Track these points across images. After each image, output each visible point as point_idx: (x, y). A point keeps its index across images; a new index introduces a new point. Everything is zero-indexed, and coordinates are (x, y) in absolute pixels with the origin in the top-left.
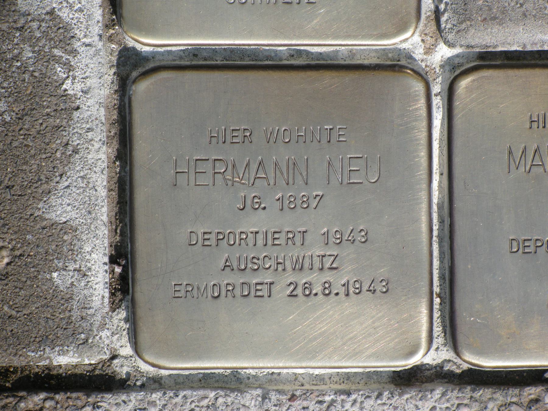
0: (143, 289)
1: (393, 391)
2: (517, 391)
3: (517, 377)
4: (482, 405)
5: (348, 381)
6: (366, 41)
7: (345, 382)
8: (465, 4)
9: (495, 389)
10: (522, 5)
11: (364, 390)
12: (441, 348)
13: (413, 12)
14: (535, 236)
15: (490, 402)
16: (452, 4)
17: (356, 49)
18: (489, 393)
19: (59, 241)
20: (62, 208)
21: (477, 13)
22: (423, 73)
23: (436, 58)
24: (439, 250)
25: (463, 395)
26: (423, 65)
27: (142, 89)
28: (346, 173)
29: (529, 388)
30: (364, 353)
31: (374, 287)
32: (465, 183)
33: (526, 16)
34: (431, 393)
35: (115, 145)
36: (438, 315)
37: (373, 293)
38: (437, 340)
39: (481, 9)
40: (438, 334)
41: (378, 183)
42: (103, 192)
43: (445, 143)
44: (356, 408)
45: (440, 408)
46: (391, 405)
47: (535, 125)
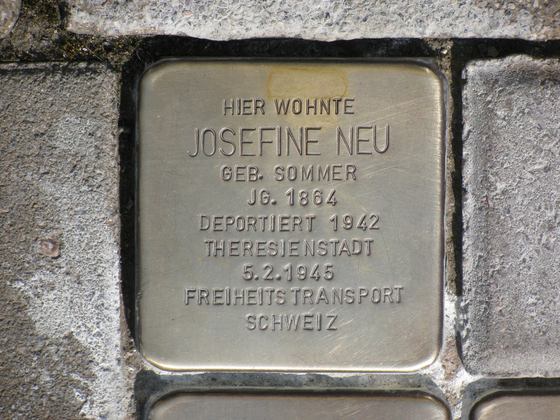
13: (435, 339)
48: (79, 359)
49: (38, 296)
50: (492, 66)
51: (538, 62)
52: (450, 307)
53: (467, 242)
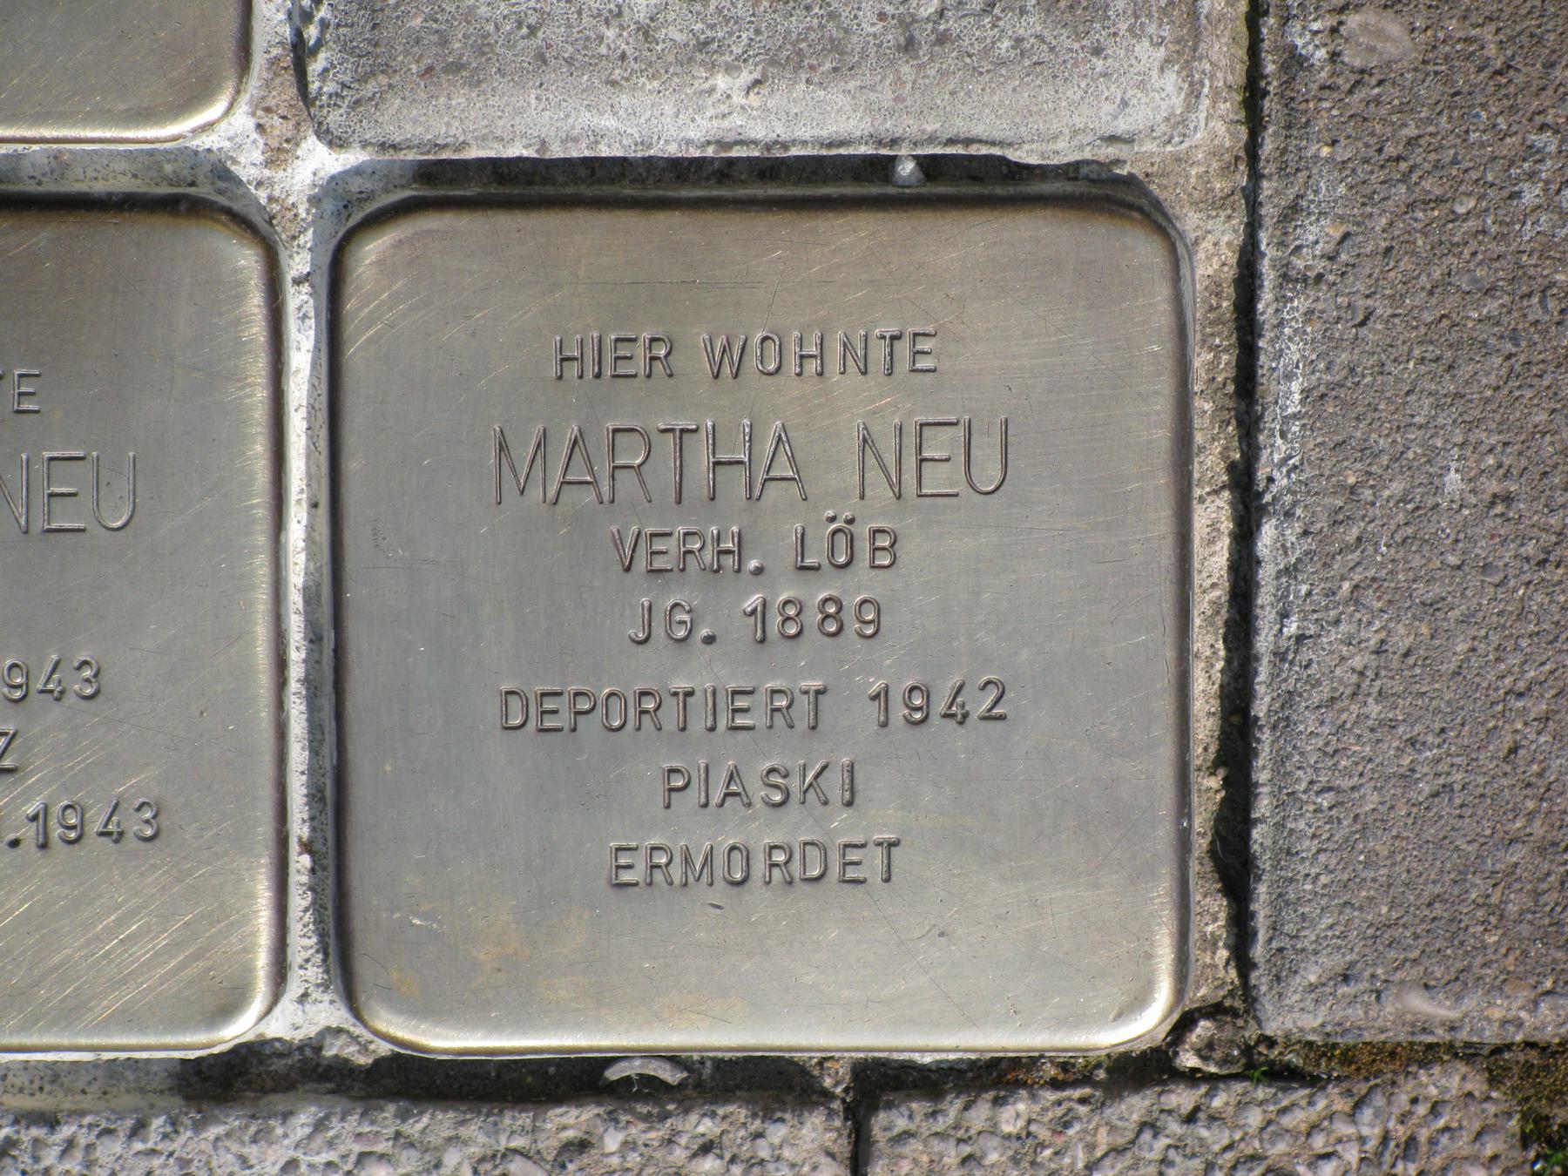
1: (177, 1117)
2: (525, 1118)
3: (529, 1079)
4: (427, 1158)
5: (55, 1087)
6: (94, 128)
7: (47, 1087)
8: (375, 26)
9: (465, 1113)
10: (533, 31)
11: (96, 1113)
12: (314, 996)
13: (229, 49)
14: (572, 683)
15: (451, 1149)
16: (338, 25)
17: (70, 151)
18: (447, 1124)
21: (407, 53)
22: (258, 220)
23: (297, 178)
24: (309, 720)
25: (375, 1128)
26: (262, 195)
28: (39, 501)
29: (558, 1111)
30: (92, 1009)
31: (118, 825)
32: (375, 531)
33: (545, 62)
34: (284, 1123)
36: (305, 903)
37: (117, 841)
38: (302, 972)
39: (418, 41)
40: (306, 955)
41: (129, 531)
43: (323, 416)
44: (73, 1165)
45: (310, 1165)
46: (171, 1154)
47: (572, 370)
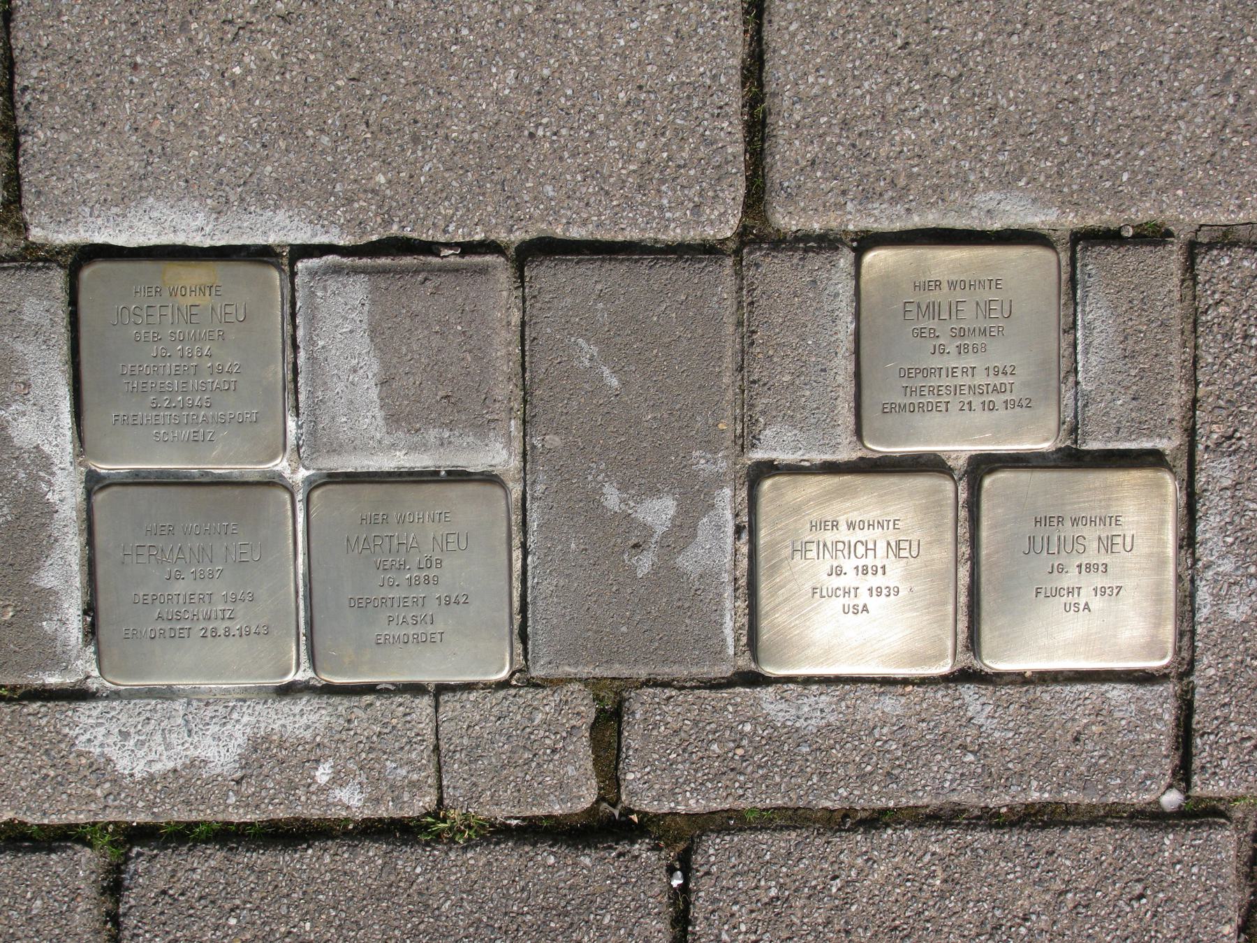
0: (103, 631)
13: (281, 446)
19: (46, 601)
20: (48, 579)
27: (99, 498)
35: (85, 535)
42: (76, 568)
48: (44, 462)
49: (15, 419)
50: (314, 263)
51: (345, 260)
52: (291, 424)
53: (301, 381)
